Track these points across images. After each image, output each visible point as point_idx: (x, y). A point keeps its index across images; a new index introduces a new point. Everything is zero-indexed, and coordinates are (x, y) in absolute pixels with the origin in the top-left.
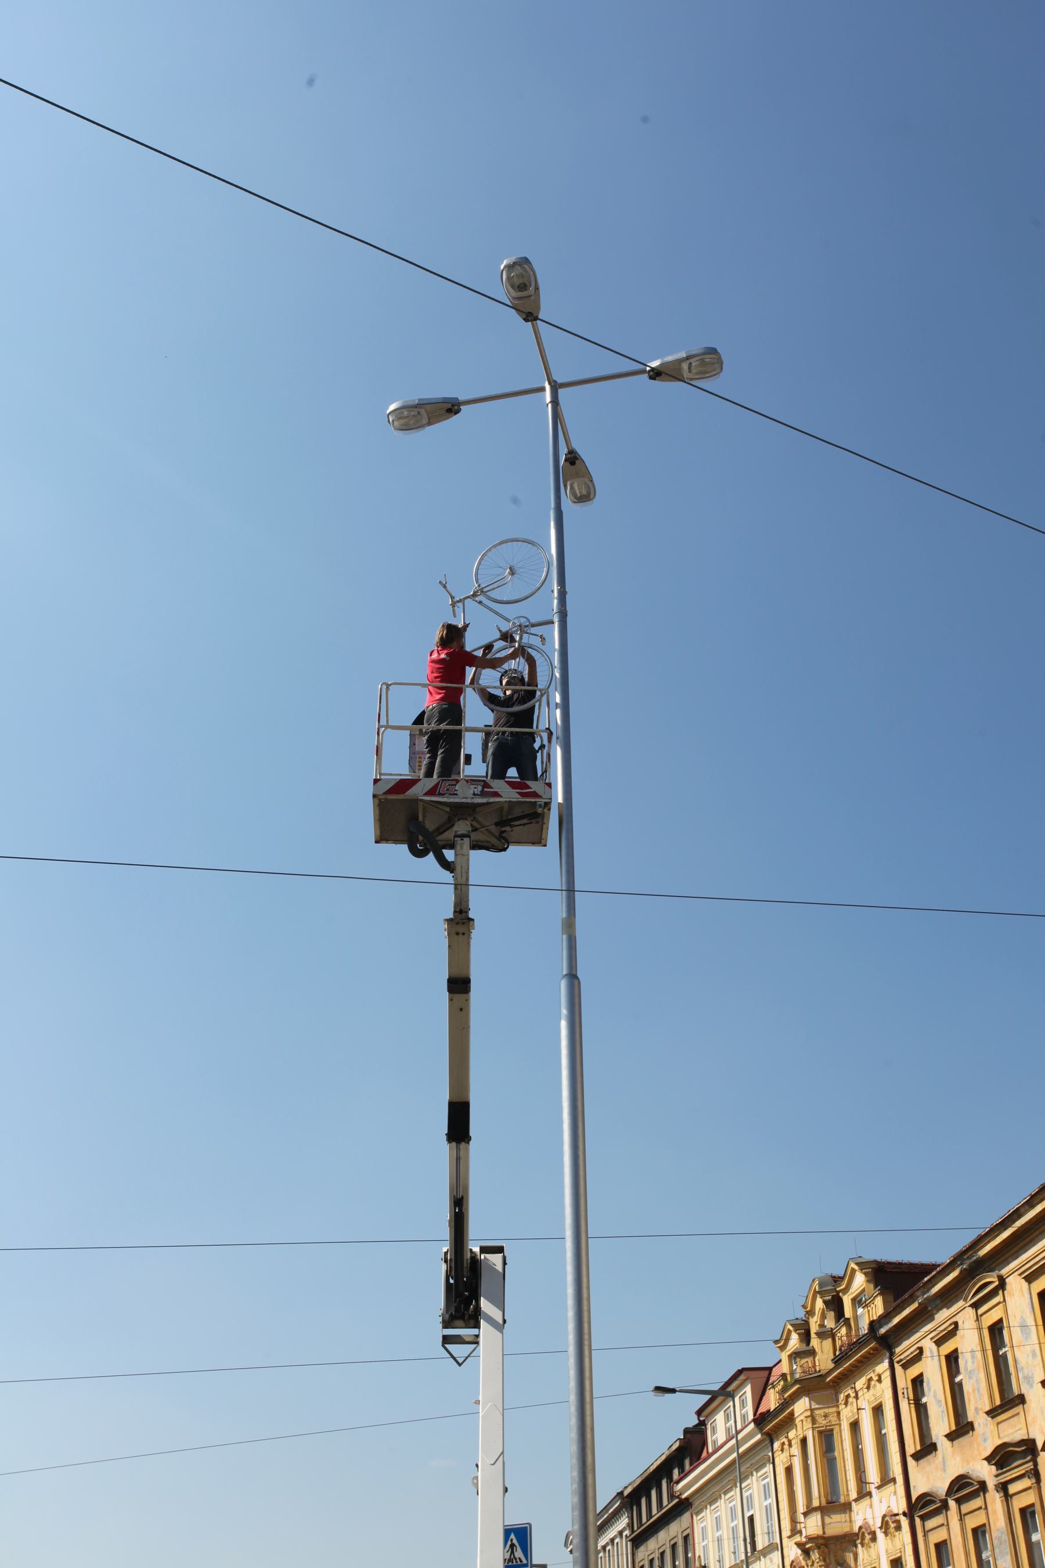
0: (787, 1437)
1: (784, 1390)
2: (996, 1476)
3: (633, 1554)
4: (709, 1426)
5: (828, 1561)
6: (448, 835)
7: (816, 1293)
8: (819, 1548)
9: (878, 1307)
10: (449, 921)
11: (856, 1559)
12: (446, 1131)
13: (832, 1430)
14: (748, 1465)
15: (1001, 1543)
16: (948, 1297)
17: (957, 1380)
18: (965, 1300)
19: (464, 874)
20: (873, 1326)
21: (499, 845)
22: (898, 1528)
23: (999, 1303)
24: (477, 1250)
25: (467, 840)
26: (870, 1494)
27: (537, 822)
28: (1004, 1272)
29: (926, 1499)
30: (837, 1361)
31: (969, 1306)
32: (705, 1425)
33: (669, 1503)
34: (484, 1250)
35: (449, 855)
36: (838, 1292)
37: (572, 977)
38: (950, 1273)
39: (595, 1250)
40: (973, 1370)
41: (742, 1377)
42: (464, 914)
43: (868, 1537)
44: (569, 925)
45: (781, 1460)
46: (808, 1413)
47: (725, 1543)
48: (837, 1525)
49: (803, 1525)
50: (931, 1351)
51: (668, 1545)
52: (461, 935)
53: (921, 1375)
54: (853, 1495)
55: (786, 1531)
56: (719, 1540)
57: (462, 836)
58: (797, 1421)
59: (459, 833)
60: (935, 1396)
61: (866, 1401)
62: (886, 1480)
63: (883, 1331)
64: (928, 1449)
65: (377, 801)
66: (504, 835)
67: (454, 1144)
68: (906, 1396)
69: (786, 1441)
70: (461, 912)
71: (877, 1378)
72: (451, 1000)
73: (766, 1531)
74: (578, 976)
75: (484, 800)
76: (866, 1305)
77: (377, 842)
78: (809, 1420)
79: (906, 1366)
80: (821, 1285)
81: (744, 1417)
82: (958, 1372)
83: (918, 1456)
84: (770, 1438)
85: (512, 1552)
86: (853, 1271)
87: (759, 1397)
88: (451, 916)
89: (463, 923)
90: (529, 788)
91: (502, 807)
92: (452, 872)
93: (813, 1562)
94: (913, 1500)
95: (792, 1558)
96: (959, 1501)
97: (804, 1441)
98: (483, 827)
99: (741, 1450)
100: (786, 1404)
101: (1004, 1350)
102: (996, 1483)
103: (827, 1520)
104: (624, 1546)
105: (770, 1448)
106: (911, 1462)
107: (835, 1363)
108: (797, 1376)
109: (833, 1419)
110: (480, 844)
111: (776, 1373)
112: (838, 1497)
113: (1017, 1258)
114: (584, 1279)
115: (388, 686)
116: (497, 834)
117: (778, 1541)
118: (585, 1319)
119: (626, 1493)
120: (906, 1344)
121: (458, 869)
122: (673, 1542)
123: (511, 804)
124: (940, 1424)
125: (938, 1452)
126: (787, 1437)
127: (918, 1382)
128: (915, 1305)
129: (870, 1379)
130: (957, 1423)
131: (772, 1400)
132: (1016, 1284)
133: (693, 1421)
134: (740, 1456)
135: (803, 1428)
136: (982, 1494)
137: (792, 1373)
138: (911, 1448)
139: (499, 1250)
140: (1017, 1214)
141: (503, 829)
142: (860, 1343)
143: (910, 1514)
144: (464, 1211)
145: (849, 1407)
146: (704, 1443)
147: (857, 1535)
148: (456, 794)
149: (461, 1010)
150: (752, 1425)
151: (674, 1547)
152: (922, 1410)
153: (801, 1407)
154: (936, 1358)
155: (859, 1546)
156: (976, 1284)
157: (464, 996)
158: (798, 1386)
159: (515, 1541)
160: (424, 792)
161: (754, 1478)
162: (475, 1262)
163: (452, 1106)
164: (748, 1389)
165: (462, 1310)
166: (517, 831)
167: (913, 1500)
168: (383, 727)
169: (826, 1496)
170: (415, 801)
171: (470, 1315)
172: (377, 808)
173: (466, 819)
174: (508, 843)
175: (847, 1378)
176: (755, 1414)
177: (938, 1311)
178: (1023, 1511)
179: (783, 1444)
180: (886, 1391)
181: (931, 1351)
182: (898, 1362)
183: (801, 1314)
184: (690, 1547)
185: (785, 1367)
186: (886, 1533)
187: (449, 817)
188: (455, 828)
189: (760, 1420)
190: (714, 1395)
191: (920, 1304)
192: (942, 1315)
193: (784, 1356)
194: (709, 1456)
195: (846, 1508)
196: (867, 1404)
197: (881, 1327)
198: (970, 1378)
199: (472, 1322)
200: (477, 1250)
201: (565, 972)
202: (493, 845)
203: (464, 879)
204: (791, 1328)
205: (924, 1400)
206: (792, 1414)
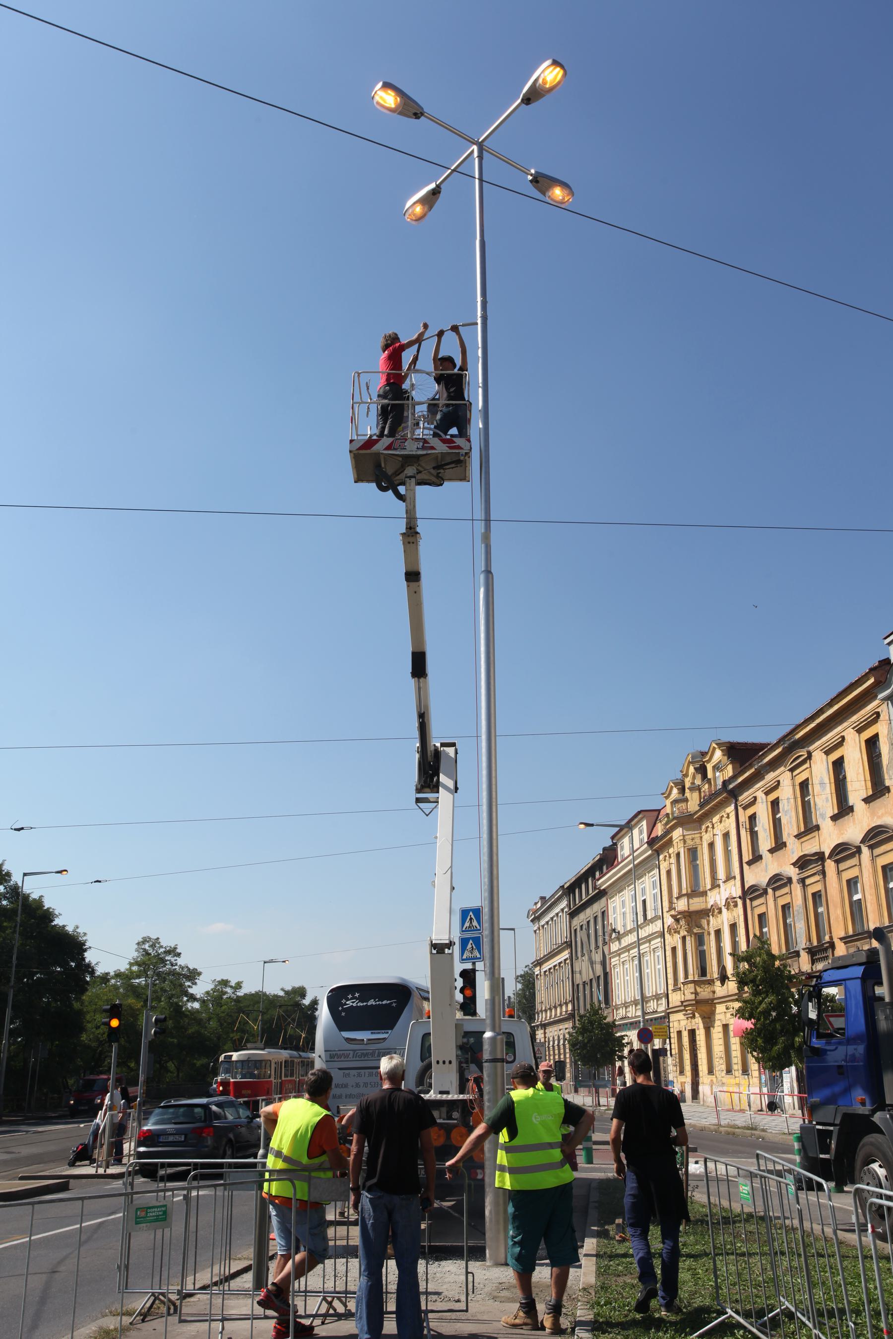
0: (668, 852)
1: (666, 824)
2: (798, 874)
3: (570, 922)
4: (619, 846)
5: (690, 925)
6: (402, 476)
7: (690, 763)
8: (685, 918)
9: (729, 771)
10: (403, 534)
11: (708, 924)
12: (411, 671)
13: (697, 848)
14: (643, 869)
15: (799, 914)
16: (774, 765)
17: (778, 816)
18: (785, 767)
19: (412, 503)
20: (725, 783)
21: (438, 482)
22: (736, 905)
23: (807, 768)
24: (438, 745)
25: (413, 480)
26: (719, 886)
27: (461, 466)
28: (811, 748)
29: (754, 889)
30: (702, 806)
31: (788, 770)
32: (617, 845)
33: (593, 892)
34: (443, 745)
35: (402, 489)
36: (704, 762)
37: (488, 572)
38: (777, 749)
39: (501, 744)
40: (788, 810)
41: (640, 816)
42: (413, 530)
43: (716, 911)
44: (486, 538)
45: (664, 866)
46: (682, 838)
47: (628, 915)
48: (697, 904)
49: (676, 905)
50: (762, 799)
51: (592, 917)
52: (411, 544)
53: (755, 814)
54: (709, 886)
55: (666, 909)
56: (624, 914)
57: (410, 477)
58: (674, 842)
59: (408, 475)
60: (763, 826)
61: (719, 830)
62: (729, 878)
63: (731, 786)
64: (757, 858)
65: (352, 455)
66: (440, 475)
67: (416, 679)
68: (744, 826)
69: (667, 854)
70: (411, 528)
71: (726, 816)
72: (408, 586)
73: (653, 908)
74: (492, 571)
75: (424, 452)
76: (722, 770)
77: (355, 482)
78: (682, 842)
79: (745, 808)
80: (692, 758)
81: (641, 840)
82: (778, 812)
83: (750, 863)
84: (658, 852)
85: (471, 922)
86: (714, 749)
87: (652, 827)
88: (404, 531)
89: (412, 536)
90: (455, 442)
91: (437, 456)
92: (404, 502)
93: (681, 926)
94: (746, 889)
95: (669, 924)
96: (774, 890)
97: (678, 855)
98: (425, 470)
99: (635, 863)
100: (668, 832)
101: (808, 798)
102: (798, 878)
103: (691, 901)
104: (565, 918)
105: (657, 859)
106: (745, 866)
107: (700, 806)
108: (676, 815)
109: (698, 841)
110: (425, 481)
111: (663, 813)
112: (699, 888)
113: (820, 739)
114: (493, 765)
115: (359, 374)
116: (435, 474)
117: (661, 914)
118: (494, 790)
119: (565, 887)
120: (746, 794)
121: (408, 499)
122: (595, 915)
123: (443, 454)
124: (765, 842)
125: (763, 860)
126: (668, 852)
127: (753, 818)
128: (753, 770)
129: (722, 816)
130: (776, 842)
131: (659, 830)
132: (818, 757)
133: (609, 843)
134: (635, 866)
135: (678, 846)
136: (789, 885)
137: (673, 813)
138: (746, 858)
139: (453, 745)
140: (821, 711)
141: (439, 471)
142: (716, 794)
143: (743, 897)
144: (426, 721)
145: (708, 834)
146: (616, 857)
147: (710, 910)
148: (405, 449)
149: (415, 592)
150: (646, 845)
151: (596, 918)
152: (755, 835)
153: (677, 834)
154: (765, 803)
155: (711, 916)
156: (792, 757)
157: (417, 583)
158: (675, 821)
159: (473, 916)
160: (384, 448)
161: (647, 877)
162: (437, 754)
163: (414, 654)
164: (644, 823)
165: (428, 782)
166: (448, 472)
167: (746, 889)
168: (357, 403)
169: (691, 887)
170: (378, 454)
171: (433, 785)
172: (353, 460)
173: (413, 465)
174: (443, 480)
175: (707, 815)
176: (648, 838)
177: (767, 774)
178: (814, 895)
179: (666, 856)
180: (732, 824)
181: (762, 799)
182: (740, 806)
183: (679, 776)
184: (606, 918)
185: (668, 810)
186: (728, 909)
187: (402, 464)
188: (406, 472)
189: (651, 842)
190: (622, 828)
191: (755, 769)
192: (770, 776)
193: (668, 803)
194: (619, 864)
195: (704, 894)
196: (719, 832)
197: (730, 784)
198: (786, 815)
199: (435, 789)
200: (438, 745)
201: (483, 569)
202: (434, 482)
203: (412, 506)
204: (673, 785)
205: (756, 829)
206: (671, 838)
